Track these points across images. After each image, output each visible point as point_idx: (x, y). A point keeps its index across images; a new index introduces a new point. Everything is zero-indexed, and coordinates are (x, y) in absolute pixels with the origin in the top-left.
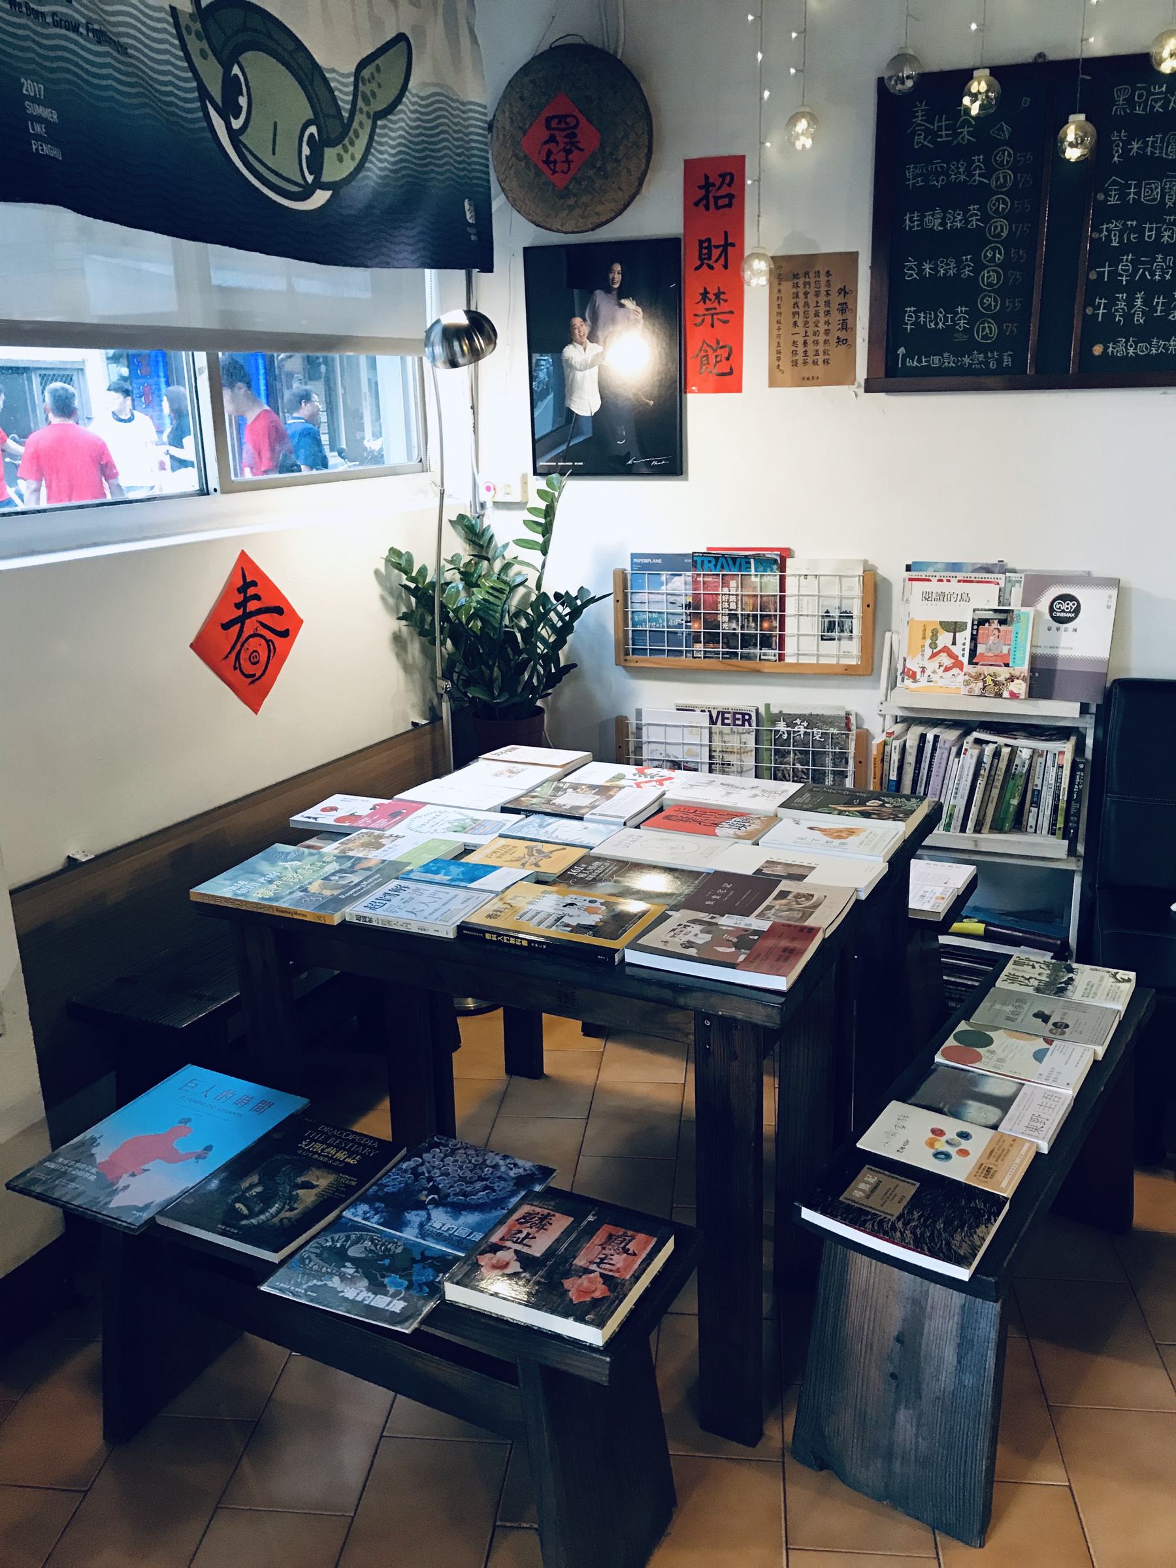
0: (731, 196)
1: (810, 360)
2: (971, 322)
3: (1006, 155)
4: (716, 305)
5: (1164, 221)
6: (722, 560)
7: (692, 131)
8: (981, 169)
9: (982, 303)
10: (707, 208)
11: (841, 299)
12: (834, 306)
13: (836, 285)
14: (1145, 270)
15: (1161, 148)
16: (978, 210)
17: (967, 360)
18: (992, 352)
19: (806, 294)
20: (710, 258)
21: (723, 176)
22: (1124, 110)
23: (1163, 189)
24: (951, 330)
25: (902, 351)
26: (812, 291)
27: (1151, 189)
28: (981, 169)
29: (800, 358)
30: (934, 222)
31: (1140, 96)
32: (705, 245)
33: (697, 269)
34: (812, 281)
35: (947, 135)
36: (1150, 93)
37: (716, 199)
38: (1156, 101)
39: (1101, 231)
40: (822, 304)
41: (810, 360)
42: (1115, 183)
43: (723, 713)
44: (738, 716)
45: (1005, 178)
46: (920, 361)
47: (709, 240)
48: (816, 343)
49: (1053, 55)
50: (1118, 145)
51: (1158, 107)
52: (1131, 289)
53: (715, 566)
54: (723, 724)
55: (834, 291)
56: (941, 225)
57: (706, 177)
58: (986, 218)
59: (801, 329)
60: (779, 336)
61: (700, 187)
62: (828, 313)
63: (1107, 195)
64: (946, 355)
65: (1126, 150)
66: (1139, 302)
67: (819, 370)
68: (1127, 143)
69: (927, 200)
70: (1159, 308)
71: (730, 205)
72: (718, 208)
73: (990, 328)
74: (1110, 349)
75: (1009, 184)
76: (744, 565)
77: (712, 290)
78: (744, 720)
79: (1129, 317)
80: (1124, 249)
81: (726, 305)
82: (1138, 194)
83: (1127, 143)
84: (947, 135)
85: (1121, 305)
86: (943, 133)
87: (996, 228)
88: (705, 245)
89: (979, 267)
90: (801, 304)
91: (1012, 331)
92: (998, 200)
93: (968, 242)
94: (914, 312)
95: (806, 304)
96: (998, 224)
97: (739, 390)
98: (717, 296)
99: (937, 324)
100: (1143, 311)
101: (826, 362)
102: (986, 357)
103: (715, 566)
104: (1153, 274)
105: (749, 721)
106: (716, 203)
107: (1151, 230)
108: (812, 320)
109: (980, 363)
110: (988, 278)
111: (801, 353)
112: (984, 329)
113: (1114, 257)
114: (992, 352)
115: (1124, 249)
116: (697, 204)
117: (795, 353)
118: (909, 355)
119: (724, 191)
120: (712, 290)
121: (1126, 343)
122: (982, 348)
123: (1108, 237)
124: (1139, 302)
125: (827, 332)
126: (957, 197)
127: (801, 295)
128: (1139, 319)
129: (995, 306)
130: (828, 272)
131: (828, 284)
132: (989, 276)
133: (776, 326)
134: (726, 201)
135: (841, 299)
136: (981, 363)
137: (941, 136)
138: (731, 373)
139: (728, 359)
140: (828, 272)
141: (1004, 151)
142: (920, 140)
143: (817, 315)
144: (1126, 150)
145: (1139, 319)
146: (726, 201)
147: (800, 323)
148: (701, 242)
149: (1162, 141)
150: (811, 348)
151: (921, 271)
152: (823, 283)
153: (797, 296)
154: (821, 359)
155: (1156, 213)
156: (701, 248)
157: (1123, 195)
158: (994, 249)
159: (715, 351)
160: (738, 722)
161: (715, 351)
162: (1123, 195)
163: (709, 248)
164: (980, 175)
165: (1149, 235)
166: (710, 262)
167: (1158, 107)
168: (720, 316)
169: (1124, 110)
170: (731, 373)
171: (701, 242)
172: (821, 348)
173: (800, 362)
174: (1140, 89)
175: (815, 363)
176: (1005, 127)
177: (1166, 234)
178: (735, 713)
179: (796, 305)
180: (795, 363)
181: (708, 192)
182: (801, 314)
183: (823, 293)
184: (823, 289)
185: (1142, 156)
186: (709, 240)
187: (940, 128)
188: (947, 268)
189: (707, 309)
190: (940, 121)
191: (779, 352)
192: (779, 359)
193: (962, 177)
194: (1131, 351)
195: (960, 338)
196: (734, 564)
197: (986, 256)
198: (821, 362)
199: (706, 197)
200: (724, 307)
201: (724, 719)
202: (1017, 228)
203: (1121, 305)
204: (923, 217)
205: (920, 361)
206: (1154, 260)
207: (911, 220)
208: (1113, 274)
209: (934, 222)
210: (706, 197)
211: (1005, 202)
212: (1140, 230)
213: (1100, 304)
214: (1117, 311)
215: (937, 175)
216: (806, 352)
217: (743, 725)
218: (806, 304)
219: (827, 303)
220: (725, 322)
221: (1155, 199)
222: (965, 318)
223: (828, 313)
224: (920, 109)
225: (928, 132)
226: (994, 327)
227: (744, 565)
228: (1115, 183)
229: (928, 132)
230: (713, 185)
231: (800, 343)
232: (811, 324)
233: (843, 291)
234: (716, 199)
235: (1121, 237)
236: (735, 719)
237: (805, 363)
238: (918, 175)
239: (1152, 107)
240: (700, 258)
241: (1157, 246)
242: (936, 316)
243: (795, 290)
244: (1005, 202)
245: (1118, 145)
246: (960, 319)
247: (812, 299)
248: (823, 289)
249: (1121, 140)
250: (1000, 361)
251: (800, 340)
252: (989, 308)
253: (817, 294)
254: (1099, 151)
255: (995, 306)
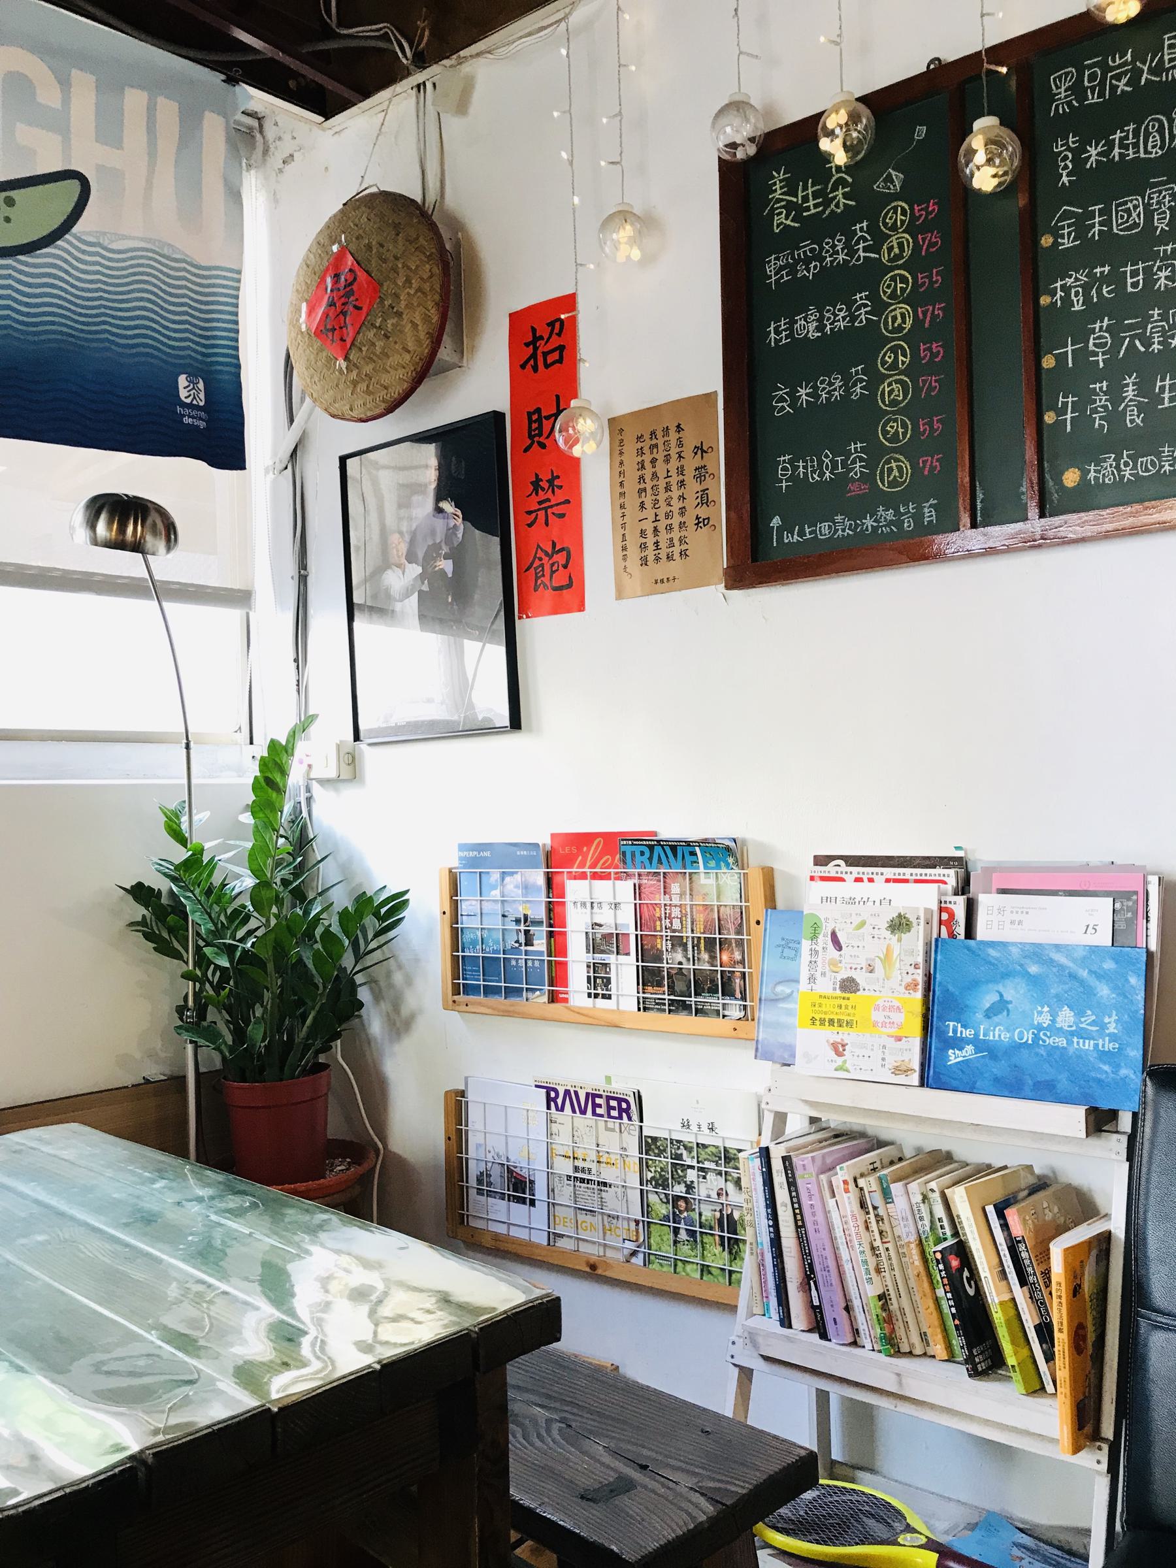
0: (561, 348)
1: (663, 556)
2: (872, 464)
3: (898, 214)
4: (549, 495)
5: (1155, 256)
6: (658, 849)
7: (512, 284)
8: (865, 240)
9: (885, 432)
10: (535, 369)
11: (698, 461)
12: (690, 472)
13: (690, 443)
14: (1132, 338)
15: (1136, 145)
16: (867, 298)
17: (869, 522)
18: (906, 505)
19: (654, 461)
20: (540, 435)
21: (551, 324)
22: (1069, 104)
23: (1147, 206)
24: (841, 481)
25: (776, 522)
26: (660, 456)
27: (1128, 211)
28: (865, 240)
29: (650, 553)
30: (808, 327)
31: (1092, 77)
32: (535, 417)
33: (526, 450)
34: (660, 442)
35: (816, 206)
36: (1106, 69)
37: (545, 354)
38: (1118, 77)
39: (1053, 293)
40: (673, 472)
41: (663, 556)
42: (1066, 215)
43: (595, 1096)
44: (613, 1103)
45: (901, 245)
46: (801, 533)
47: (538, 411)
48: (669, 528)
49: (950, 55)
50: (1065, 158)
51: (1122, 86)
52: (1114, 373)
53: (650, 859)
54: (594, 1113)
55: (688, 452)
56: (818, 329)
57: (534, 330)
58: (879, 307)
59: (649, 513)
60: (623, 525)
61: (527, 345)
62: (682, 484)
63: (1057, 235)
64: (839, 518)
65: (1079, 162)
66: (1130, 392)
67: (675, 568)
68: (1078, 152)
69: (797, 297)
70: (1166, 395)
71: (560, 360)
72: (547, 366)
73: (900, 469)
74: (1092, 475)
75: (907, 253)
76: (688, 858)
77: (545, 476)
78: (621, 1110)
79: (1115, 417)
80: (1094, 311)
81: (559, 482)
82: (1107, 223)
83: (1078, 152)
84: (816, 206)
85: (1102, 400)
86: (811, 203)
87: (894, 319)
88: (535, 417)
89: (875, 380)
90: (648, 478)
91: (932, 468)
92: (893, 279)
93: (860, 346)
94: (791, 462)
95: (655, 476)
96: (898, 312)
97: (581, 607)
98: (551, 482)
99: (822, 475)
100: (1140, 407)
101: (684, 554)
102: (897, 513)
103: (650, 859)
104: (1147, 343)
105: (627, 1111)
106: (545, 360)
107: (1135, 274)
108: (662, 497)
109: (890, 523)
110: (890, 392)
111: (651, 547)
112: (890, 470)
113: (1080, 328)
114: (906, 505)
115: (1094, 311)
116: (523, 366)
117: (643, 547)
118: (787, 527)
119: (555, 342)
120: (545, 476)
121: (1117, 460)
122: (891, 502)
123: (1067, 300)
124: (1130, 392)
125: (683, 511)
126: (836, 285)
127: (648, 465)
128: (1134, 419)
129: (904, 434)
130: (678, 426)
131: (680, 444)
132: (892, 390)
133: (619, 513)
134: (556, 355)
135: (698, 461)
136: (891, 523)
137: (808, 209)
138: (570, 586)
139: (565, 567)
140: (678, 426)
141: (895, 209)
142: (782, 220)
143: (668, 489)
144: (1079, 162)
145: (1134, 419)
146: (556, 355)
147: (649, 504)
148: (530, 414)
149: (1136, 134)
150: (663, 537)
151: (795, 399)
152: (673, 443)
153: (643, 467)
154: (676, 550)
155: (1143, 244)
156: (530, 421)
157: (1081, 230)
158: (893, 350)
159: (551, 557)
160: (614, 1113)
161: (551, 557)
162: (1081, 230)
163: (539, 420)
164: (865, 250)
165: (1133, 282)
166: (541, 440)
167: (1122, 86)
168: (555, 510)
169: (1069, 104)
170: (570, 586)
171: (530, 414)
172: (676, 535)
173: (651, 558)
174: (1090, 67)
175: (669, 558)
176: (893, 173)
177: (1163, 274)
178: (609, 1098)
179: (642, 478)
180: (644, 562)
181: (536, 349)
182: (649, 491)
183: (674, 456)
184: (673, 452)
185: (1106, 166)
186: (538, 411)
187: (805, 199)
188: (832, 388)
189: (540, 503)
190: (805, 188)
191: (624, 549)
192: (625, 558)
193: (841, 257)
194: (1127, 473)
195: (855, 489)
196: (675, 856)
197: (884, 363)
198: (676, 556)
199: (534, 356)
200: (560, 496)
201: (595, 1106)
202: (925, 313)
203: (1102, 400)
204: (793, 322)
205: (801, 533)
206: (1147, 319)
207: (777, 332)
208: (1082, 355)
209: (808, 327)
210: (534, 356)
211: (904, 280)
212: (1117, 279)
213: (1065, 404)
214: (1095, 411)
215: (807, 262)
216: (657, 543)
217: (620, 1117)
218: (655, 476)
219: (681, 471)
220: (562, 516)
221: (1136, 225)
222: (861, 459)
223: (682, 484)
224: (779, 178)
225: (790, 206)
226: (906, 465)
227: (688, 858)
228: (1066, 215)
229: (790, 206)
230: (541, 338)
231: (650, 532)
232: (662, 503)
233: (700, 450)
234: (545, 354)
235: (1087, 295)
236: (610, 1108)
237: (657, 559)
238: (782, 268)
239: (1114, 88)
240: (531, 437)
241: (1150, 296)
242: (820, 463)
243: (639, 459)
244: (904, 280)
245: (1065, 158)
246: (854, 462)
247: (661, 468)
248: (673, 452)
249: (1069, 149)
250: (918, 517)
251: (648, 526)
252: (895, 438)
253: (667, 459)
254: (1032, 172)
255: (904, 434)
